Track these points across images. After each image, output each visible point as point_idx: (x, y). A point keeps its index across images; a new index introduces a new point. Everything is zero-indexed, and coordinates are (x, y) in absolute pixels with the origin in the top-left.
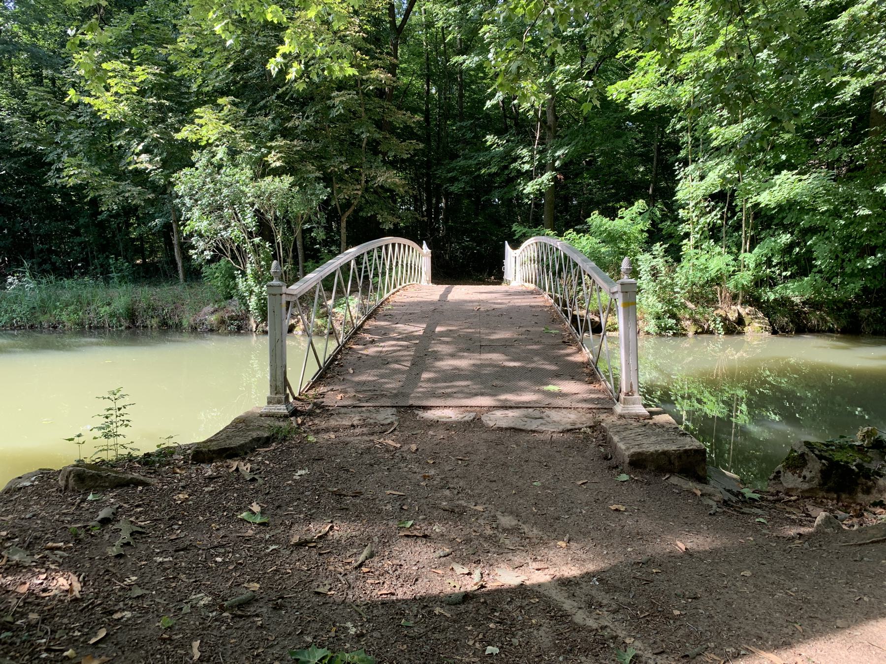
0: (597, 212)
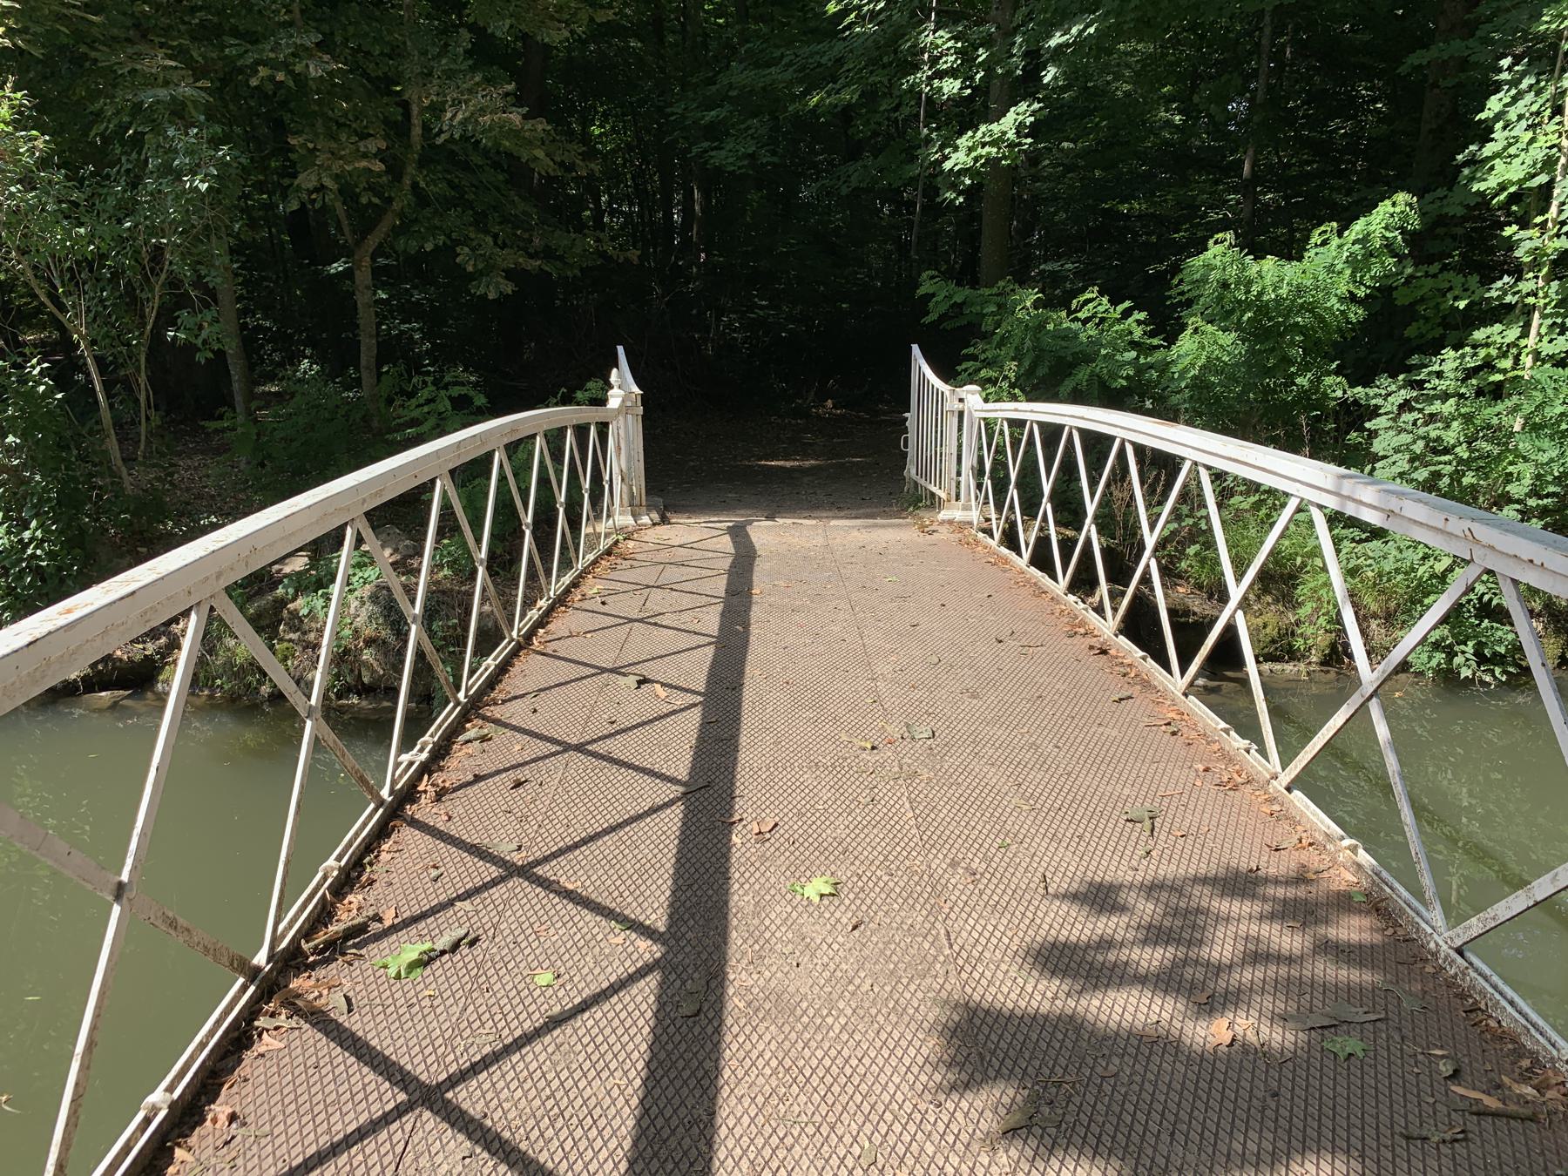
0: (1229, 236)
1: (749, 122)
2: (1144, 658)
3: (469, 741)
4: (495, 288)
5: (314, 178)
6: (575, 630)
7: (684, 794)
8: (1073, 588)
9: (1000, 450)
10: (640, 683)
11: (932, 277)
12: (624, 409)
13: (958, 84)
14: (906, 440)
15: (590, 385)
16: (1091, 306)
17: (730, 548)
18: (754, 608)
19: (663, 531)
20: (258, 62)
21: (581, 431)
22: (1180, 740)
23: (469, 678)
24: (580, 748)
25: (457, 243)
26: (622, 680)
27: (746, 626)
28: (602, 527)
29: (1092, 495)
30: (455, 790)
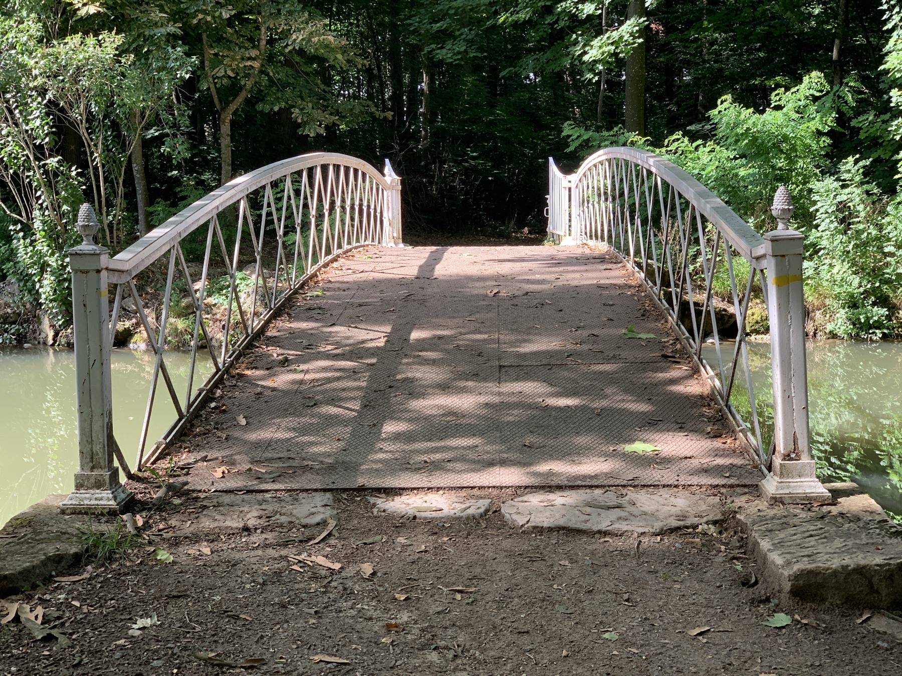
1: (462, 30)
5: (223, 70)
11: (571, 125)
13: (593, 7)
20: (198, 11)
25: (293, 106)
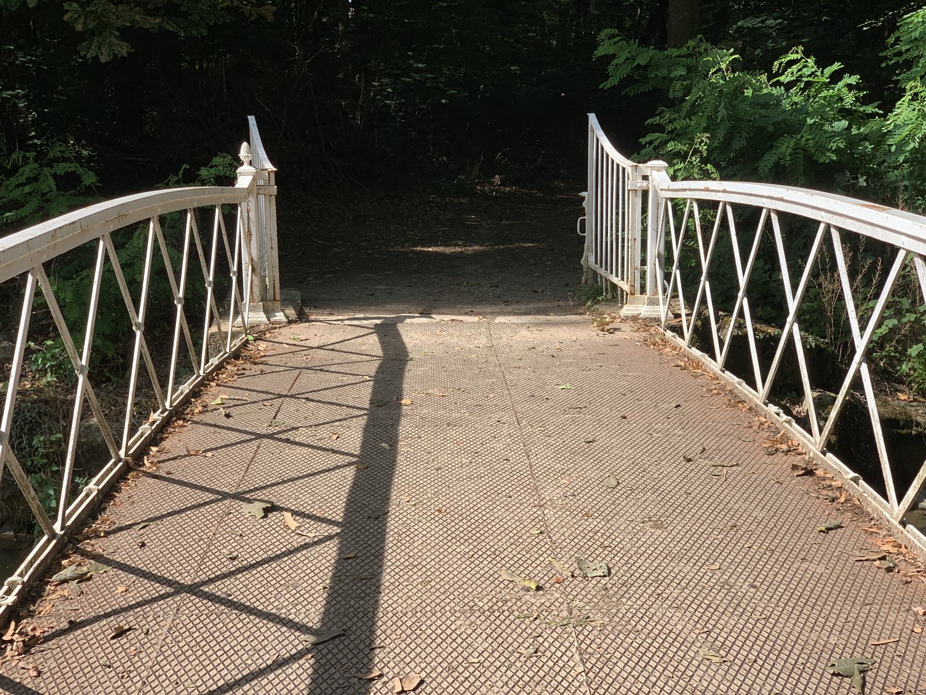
2: (855, 480)
3: (63, 582)
4: (108, 49)
6: (192, 447)
7: (315, 645)
8: (774, 396)
9: (690, 235)
10: (267, 511)
11: (611, 37)
12: (255, 189)
14: (583, 223)
15: (216, 160)
16: (795, 68)
17: (378, 351)
18: (404, 421)
19: (301, 331)
21: (204, 215)
22: (897, 578)
23: (66, 506)
24: (194, 589)
26: (246, 508)
27: (393, 442)
28: (228, 326)
29: (794, 288)
30: (47, 639)
